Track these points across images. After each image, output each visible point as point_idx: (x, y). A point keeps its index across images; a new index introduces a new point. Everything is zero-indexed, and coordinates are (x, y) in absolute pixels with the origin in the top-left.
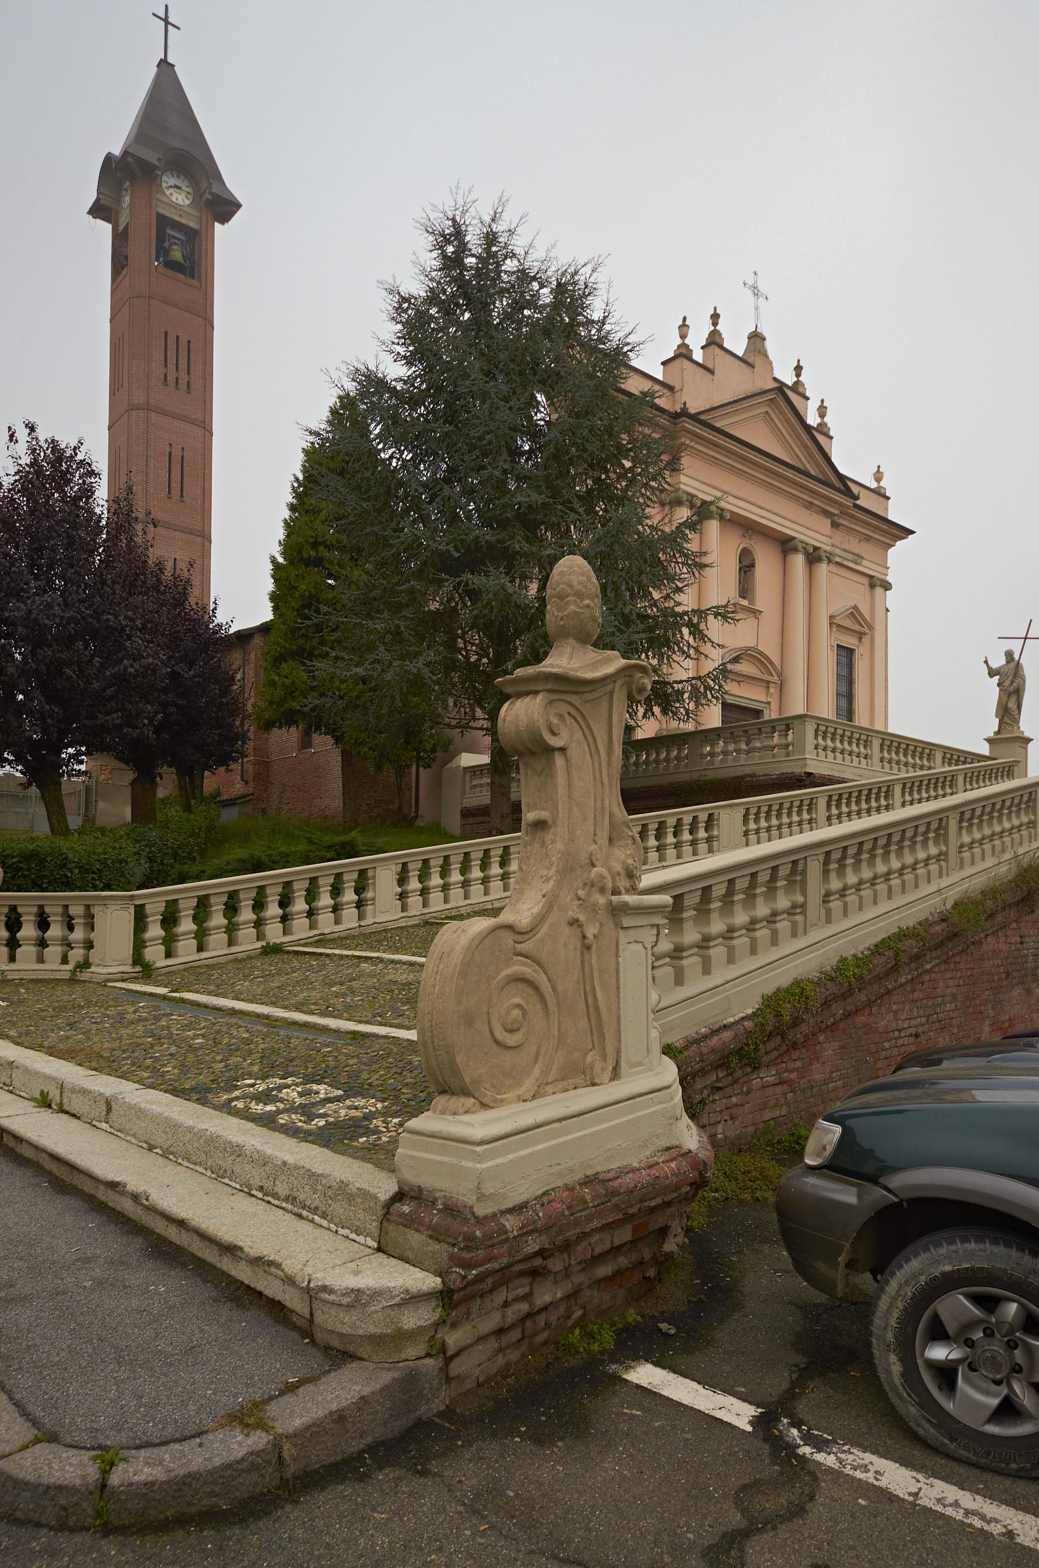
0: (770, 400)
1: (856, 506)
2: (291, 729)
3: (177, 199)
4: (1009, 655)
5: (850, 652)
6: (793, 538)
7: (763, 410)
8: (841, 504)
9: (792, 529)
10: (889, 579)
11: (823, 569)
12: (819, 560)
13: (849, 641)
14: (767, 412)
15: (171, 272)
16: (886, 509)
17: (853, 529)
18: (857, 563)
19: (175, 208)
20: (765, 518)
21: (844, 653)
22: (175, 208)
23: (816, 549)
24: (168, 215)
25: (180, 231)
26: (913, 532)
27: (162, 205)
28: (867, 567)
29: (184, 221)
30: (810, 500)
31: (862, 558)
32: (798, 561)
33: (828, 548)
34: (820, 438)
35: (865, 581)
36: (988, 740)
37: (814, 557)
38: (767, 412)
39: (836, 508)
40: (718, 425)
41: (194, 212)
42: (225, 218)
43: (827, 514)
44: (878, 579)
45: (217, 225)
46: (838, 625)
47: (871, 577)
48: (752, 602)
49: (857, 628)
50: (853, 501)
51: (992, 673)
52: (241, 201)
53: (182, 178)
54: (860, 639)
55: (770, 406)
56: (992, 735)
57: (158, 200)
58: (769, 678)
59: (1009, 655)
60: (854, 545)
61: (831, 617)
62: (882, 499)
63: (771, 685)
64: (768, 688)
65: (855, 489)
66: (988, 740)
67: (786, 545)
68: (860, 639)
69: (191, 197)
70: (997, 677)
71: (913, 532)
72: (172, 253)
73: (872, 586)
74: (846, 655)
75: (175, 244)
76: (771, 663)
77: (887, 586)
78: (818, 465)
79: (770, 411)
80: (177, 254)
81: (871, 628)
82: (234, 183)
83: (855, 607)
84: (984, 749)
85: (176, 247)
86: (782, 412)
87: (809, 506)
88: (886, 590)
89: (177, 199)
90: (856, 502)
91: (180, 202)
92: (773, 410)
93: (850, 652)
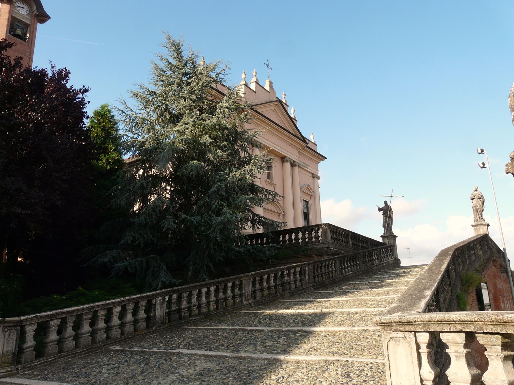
0: (276, 105)
1: (307, 147)
2: (77, 87)
3: (22, 12)
4: (386, 203)
5: (307, 203)
6: (285, 157)
7: (274, 108)
8: (302, 145)
9: (285, 153)
10: (319, 175)
11: (296, 169)
12: (296, 166)
13: (307, 198)
14: (275, 109)
15: (15, 38)
16: (316, 149)
17: (306, 155)
18: (308, 168)
19: (20, 15)
20: (276, 148)
21: (305, 203)
22: (20, 15)
23: (294, 161)
24: (17, 17)
25: (21, 24)
26: (326, 158)
27: (14, 13)
28: (310, 169)
29: (24, 20)
30: (291, 143)
31: (308, 165)
32: (288, 165)
33: (298, 162)
34: (294, 121)
35: (311, 175)
36: (382, 236)
37: (293, 165)
38: (275, 109)
39: (300, 147)
40: (259, 111)
41: (29, 18)
42: (42, 22)
43: (297, 149)
44: (315, 175)
45: (38, 24)
46: (303, 192)
47: (313, 174)
48: (272, 180)
49: (309, 193)
50: (306, 145)
51: (380, 210)
52: (51, 17)
53: (25, 4)
54: (311, 198)
55: (276, 107)
56: (383, 235)
57: (13, 11)
58: (280, 212)
59: (386, 203)
60: (307, 161)
61: (301, 188)
62: (315, 146)
63: (280, 215)
64: (279, 216)
65: (307, 141)
66: (382, 236)
67: (283, 159)
68: (311, 198)
69: (28, 12)
70: (382, 211)
71: (326, 158)
72: (17, 31)
73: (313, 177)
74: (306, 203)
75: (19, 28)
76: (280, 205)
77: (318, 178)
78: (293, 130)
79: (276, 109)
80: (19, 32)
81: (315, 194)
82: (47, 8)
83: (309, 185)
84: (381, 240)
85: (19, 29)
86: (280, 109)
87: (291, 145)
88: (318, 179)
89: (22, 12)
90: (307, 145)
91: (23, 13)
92: (277, 109)
93: (307, 203)
